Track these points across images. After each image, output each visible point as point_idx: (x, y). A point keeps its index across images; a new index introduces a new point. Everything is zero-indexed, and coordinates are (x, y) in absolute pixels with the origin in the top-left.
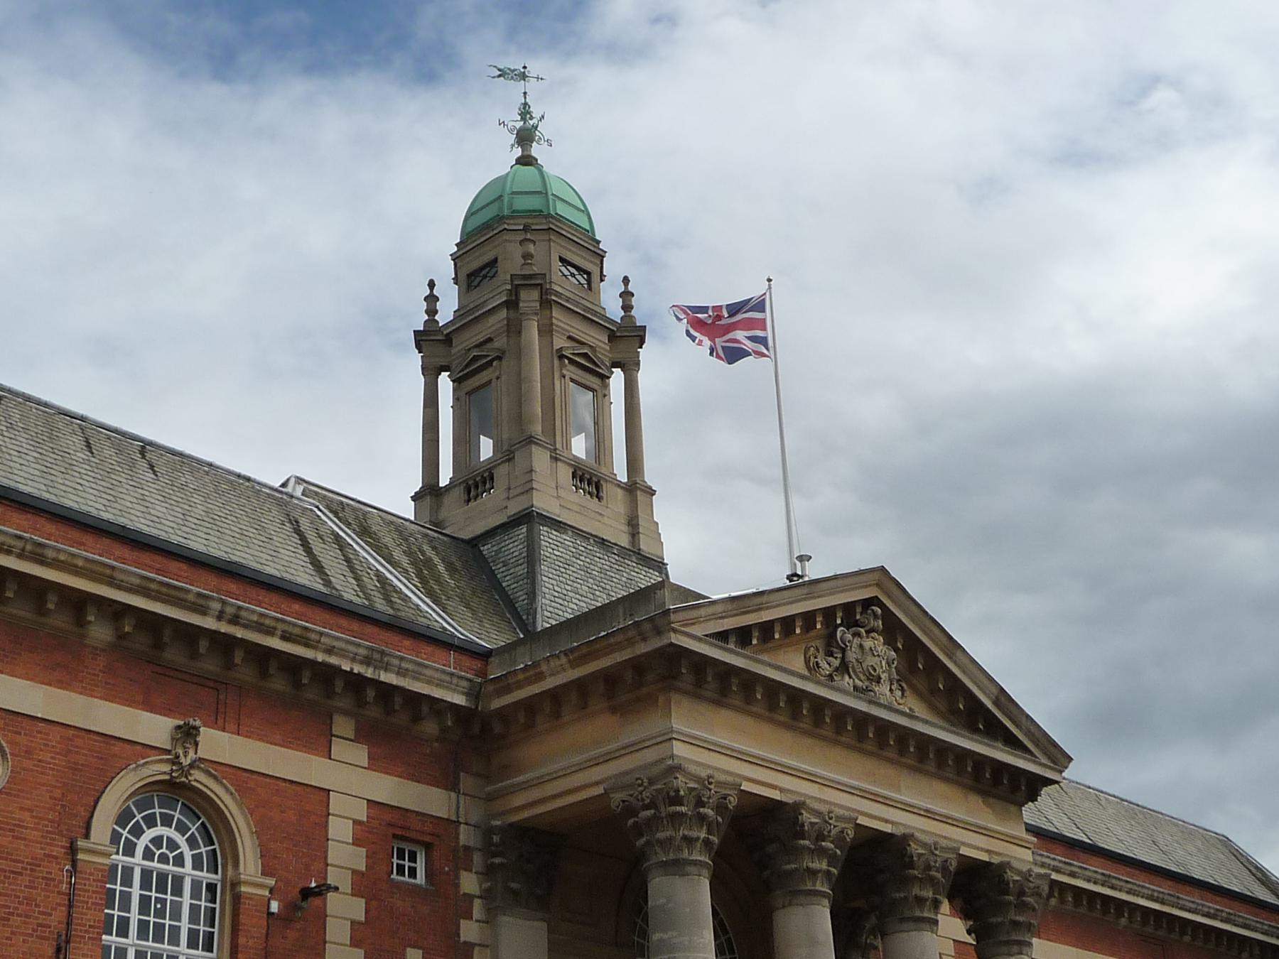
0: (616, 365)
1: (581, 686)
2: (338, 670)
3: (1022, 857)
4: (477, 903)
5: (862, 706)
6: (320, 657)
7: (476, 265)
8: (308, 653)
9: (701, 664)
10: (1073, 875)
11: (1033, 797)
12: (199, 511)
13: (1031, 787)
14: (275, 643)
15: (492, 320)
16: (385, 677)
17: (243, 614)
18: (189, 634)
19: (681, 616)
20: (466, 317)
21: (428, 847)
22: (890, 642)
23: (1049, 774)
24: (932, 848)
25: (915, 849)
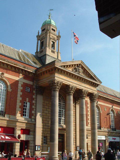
0: (57, 40)
1: (46, 71)
2: (20, 68)
3: (96, 93)
4: (35, 94)
5: (78, 75)
6: (18, 67)
7: (43, 29)
8: (17, 66)
9: (59, 69)
10: (104, 95)
11: (97, 86)
12: (8, 51)
13: (97, 85)
14: (13, 65)
15: (44, 35)
16: (25, 69)
17: (9, 62)
18: (3, 63)
19: (57, 63)
20: (42, 34)
21: (30, 88)
22: (82, 69)
23: (99, 84)
24: (85, 91)
25: (83, 91)
